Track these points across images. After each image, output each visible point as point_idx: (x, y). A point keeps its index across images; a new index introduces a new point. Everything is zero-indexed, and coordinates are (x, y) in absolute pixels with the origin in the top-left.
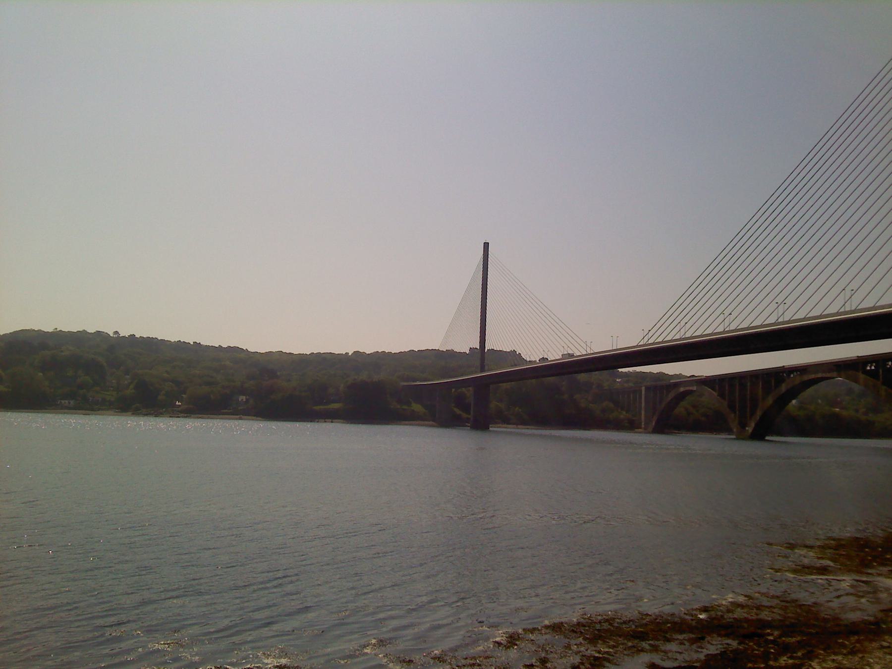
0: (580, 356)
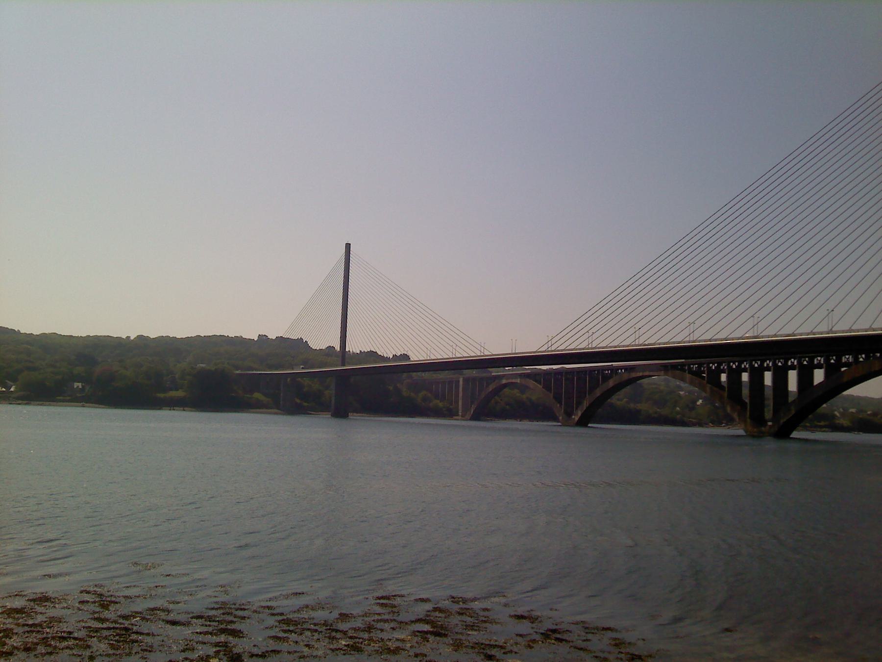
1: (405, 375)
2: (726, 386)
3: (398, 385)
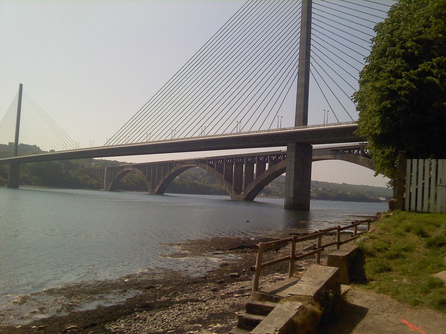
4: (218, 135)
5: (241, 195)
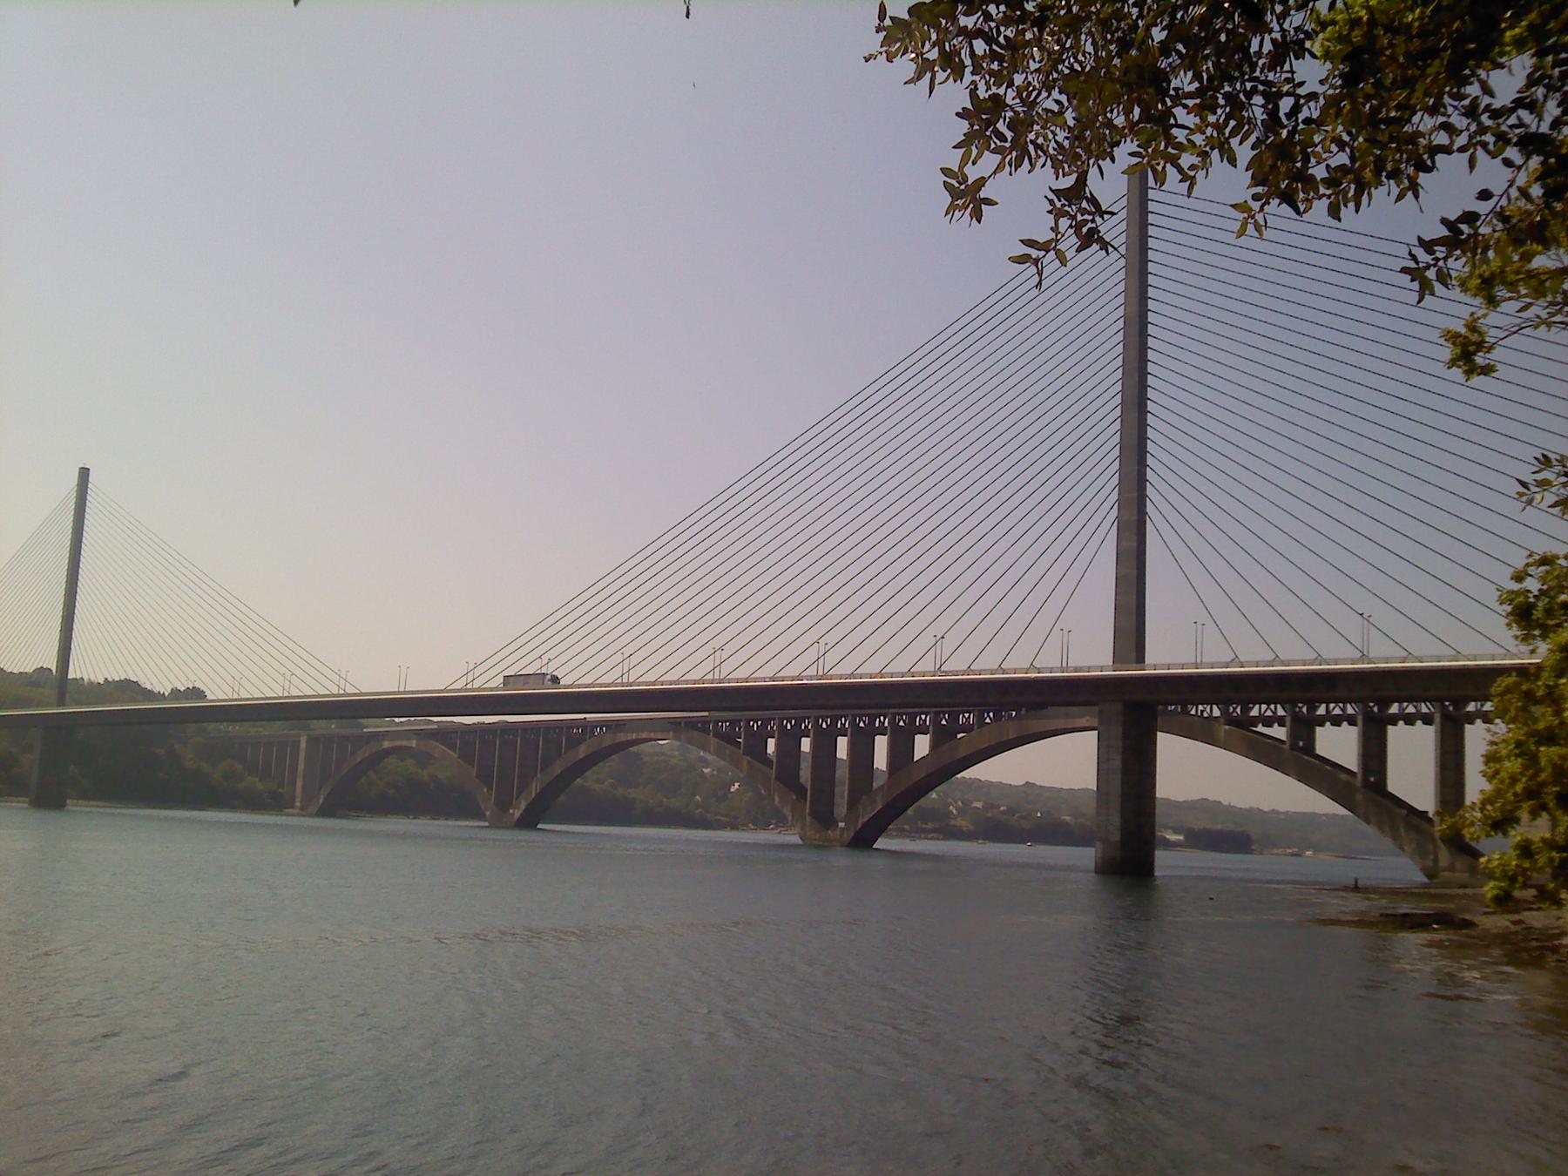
0: (355, 694)
1: (192, 727)
2: (775, 761)
3: (177, 747)
4: (687, 681)
5: (838, 832)
